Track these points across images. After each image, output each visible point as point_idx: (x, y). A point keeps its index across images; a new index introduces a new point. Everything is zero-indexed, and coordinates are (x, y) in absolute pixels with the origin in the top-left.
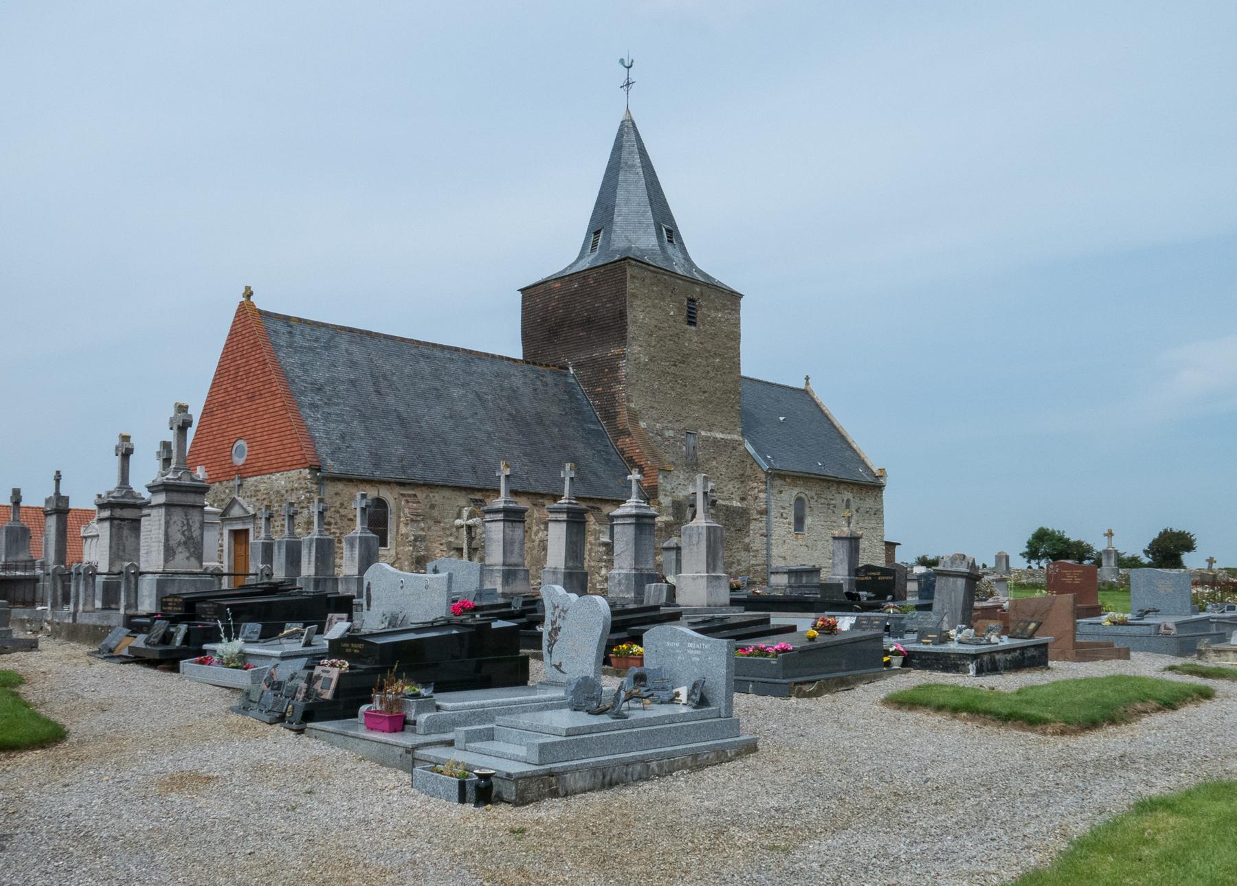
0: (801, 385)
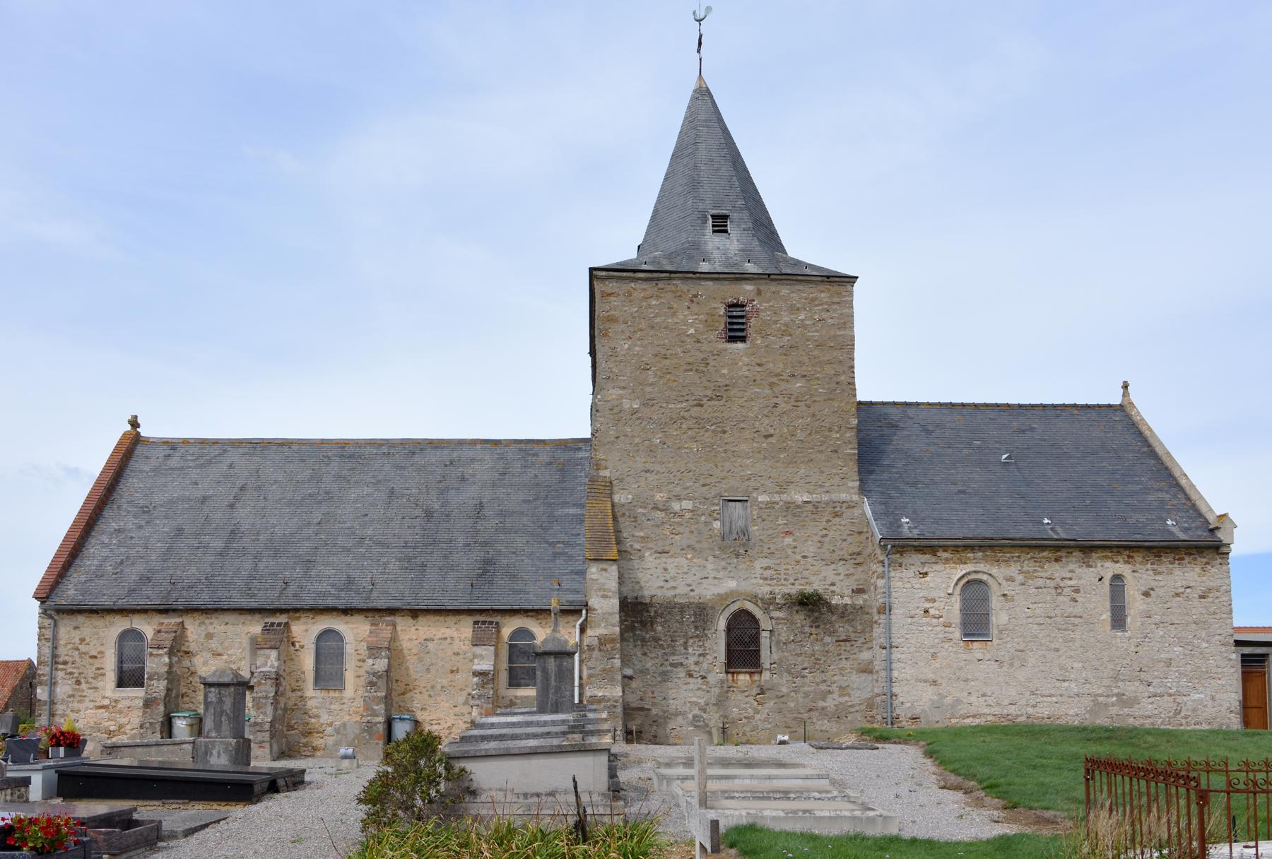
0: (1116, 400)
